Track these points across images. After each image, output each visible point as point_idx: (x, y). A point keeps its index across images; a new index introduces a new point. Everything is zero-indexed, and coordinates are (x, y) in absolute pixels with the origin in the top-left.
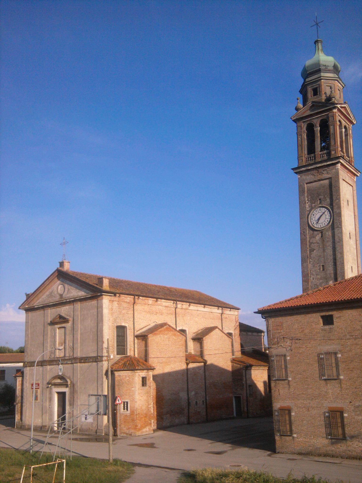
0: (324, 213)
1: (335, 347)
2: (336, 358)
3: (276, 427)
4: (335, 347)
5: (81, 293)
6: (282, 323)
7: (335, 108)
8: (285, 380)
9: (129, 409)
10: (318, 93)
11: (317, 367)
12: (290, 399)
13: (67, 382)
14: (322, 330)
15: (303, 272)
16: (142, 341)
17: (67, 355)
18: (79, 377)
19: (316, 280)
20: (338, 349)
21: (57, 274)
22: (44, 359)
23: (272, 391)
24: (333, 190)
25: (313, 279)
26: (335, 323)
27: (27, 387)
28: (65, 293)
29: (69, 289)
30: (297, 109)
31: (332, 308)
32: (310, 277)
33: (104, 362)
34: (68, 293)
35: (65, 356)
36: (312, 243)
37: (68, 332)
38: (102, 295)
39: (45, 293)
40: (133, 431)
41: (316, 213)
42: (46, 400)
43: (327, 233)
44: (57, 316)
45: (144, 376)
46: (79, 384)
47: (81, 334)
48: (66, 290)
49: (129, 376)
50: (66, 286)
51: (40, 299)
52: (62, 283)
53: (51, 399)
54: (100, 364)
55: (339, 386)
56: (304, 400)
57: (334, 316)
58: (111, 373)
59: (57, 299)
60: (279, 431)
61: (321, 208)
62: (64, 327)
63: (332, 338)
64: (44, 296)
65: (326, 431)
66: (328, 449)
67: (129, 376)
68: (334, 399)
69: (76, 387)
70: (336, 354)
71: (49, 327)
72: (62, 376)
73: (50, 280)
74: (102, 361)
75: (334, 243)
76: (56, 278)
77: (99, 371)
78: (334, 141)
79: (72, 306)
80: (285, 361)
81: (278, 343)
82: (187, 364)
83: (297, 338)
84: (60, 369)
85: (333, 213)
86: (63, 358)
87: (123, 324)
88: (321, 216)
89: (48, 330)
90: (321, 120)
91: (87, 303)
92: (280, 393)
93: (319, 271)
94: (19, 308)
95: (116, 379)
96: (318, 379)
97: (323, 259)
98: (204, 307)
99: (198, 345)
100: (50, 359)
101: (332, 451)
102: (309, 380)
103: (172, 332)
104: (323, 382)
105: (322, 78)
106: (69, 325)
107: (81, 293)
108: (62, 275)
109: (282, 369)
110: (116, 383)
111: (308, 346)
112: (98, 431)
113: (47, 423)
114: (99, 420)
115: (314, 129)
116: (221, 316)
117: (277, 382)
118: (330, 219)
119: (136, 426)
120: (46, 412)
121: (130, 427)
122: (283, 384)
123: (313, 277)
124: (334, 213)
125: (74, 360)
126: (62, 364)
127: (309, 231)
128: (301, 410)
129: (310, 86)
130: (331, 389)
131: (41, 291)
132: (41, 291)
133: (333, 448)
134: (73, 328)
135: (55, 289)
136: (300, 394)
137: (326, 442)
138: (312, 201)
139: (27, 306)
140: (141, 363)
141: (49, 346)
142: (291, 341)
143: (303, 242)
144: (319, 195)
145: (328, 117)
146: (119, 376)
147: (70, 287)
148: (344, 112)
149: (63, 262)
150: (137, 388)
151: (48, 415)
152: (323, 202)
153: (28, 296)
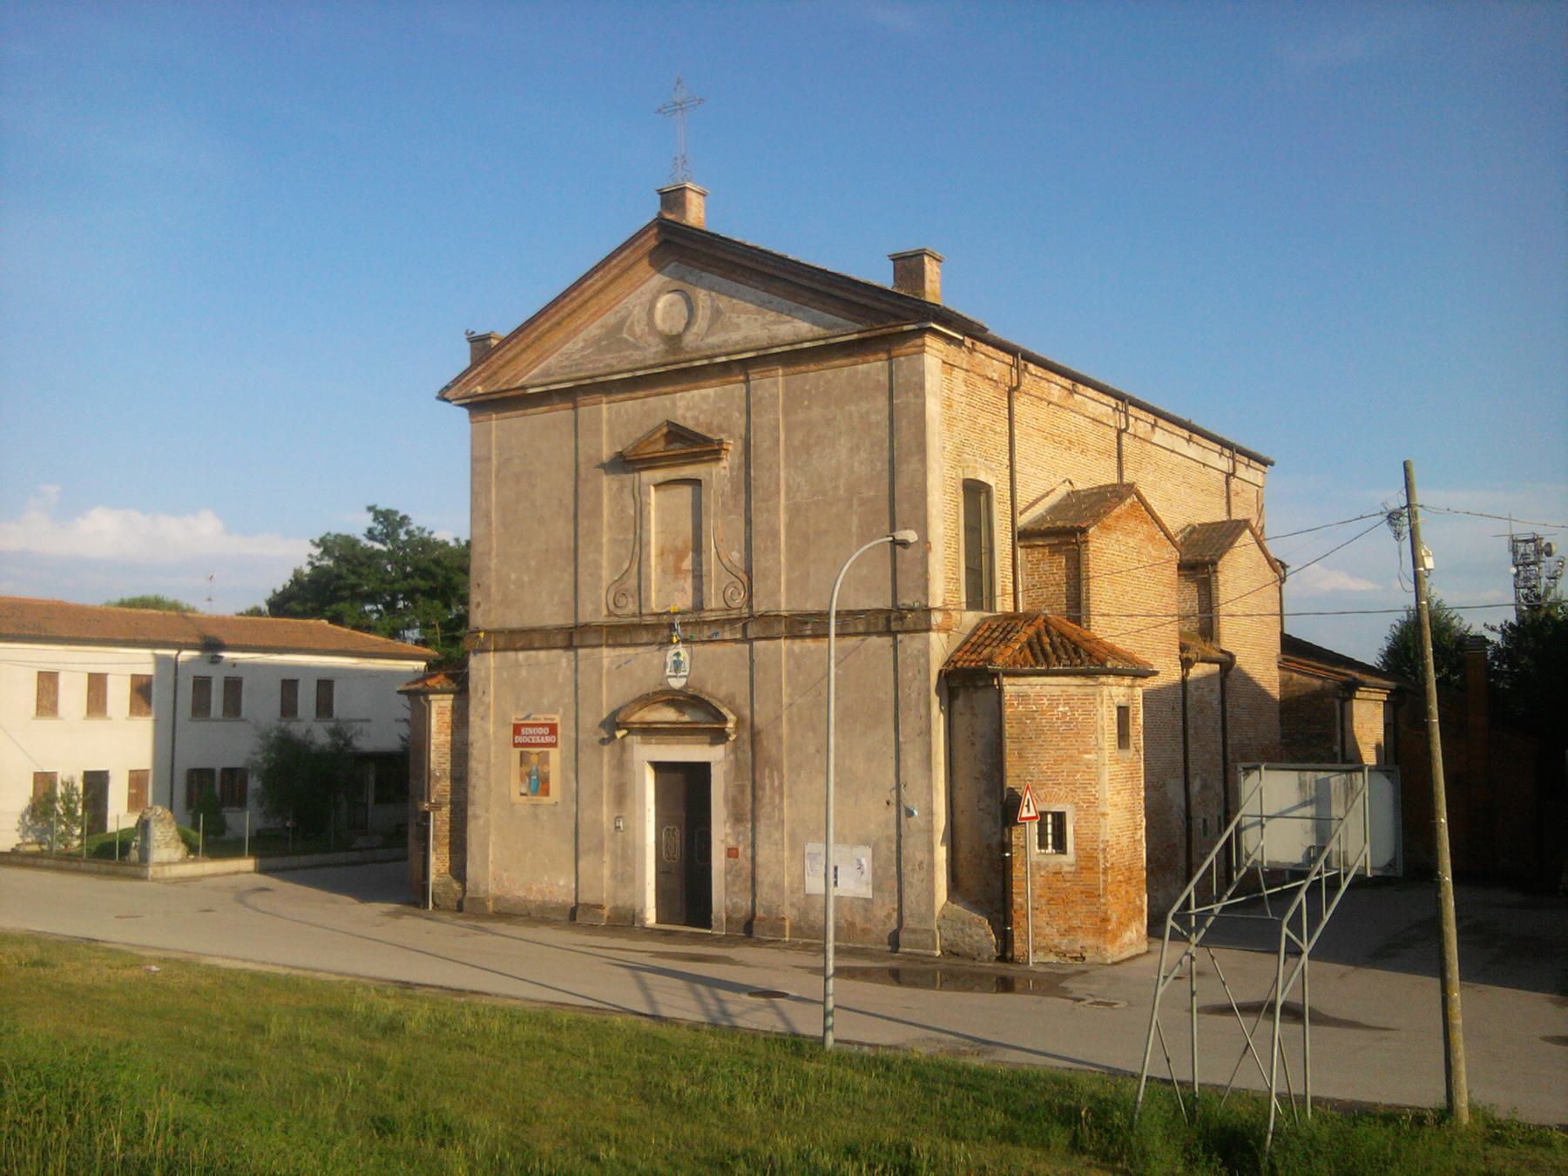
5: (797, 328)
9: (1070, 846)
13: (725, 720)
16: (1052, 553)
17: (713, 601)
18: (785, 700)
21: (653, 243)
22: (582, 620)
27: (486, 735)
28: (695, 329)
29: (717, 313)
33: (933, 636)
34: (710, 330)
35: (699, 606)
37: (711, 503)
38: (921, 332)
39: (576, 332)
40: (1090, 941)
42: (597, 795)
44: (659, 428)
45: (1123, 701)
46: (785, 729)
47: (795, 511)
48: (703, 315)
49: (1068, 700)
50: (702, 297)
51: (552, 361)
52: (676, 284)
53: (622, 794)
54: (911, 644)
58: (967, 683)
59: (651, 353)
62: (696, 483)
64: (575, 346)
67: (1068, 700)
69: (767, 743)
71: (607, 483)
72: (691, 691)
73: (615, 271)
74: (928, 629)
76: (646, 262)
77: (907, 674)
79: (736, 389)
82: (1186, 664)
84: (678, 665)
86: (690, 618)
87: (982, 478)
89: (599, 494)
91: (829, 374)
94: (442, 397)
95: (1008, 711)
98: (1189, 440)
99: (1191, 591)
100: (614, 620)
106: (719, 474)
107: (797, 328)
108: (678, 246)
110: (1009, 730)
112: (904, 936)
113: (602, 888)
114: (907, 891)
116: (1228, 484)
119: (1105, 920)
120: (599, 848)
121: (1076, 922)
125: (754, 625)
126: (685, 641)
131: (559, 324)
132: (559, 324)
134: (746, 485)
135: (639, 313)
139: (480, 389)
140: (1068, 649)
141: (605, 563)
146: (1023, 698)
147: (723, 302)
148: (536, 371)
149: (682, 190)
151: (607, 858)
153: (482, 347)
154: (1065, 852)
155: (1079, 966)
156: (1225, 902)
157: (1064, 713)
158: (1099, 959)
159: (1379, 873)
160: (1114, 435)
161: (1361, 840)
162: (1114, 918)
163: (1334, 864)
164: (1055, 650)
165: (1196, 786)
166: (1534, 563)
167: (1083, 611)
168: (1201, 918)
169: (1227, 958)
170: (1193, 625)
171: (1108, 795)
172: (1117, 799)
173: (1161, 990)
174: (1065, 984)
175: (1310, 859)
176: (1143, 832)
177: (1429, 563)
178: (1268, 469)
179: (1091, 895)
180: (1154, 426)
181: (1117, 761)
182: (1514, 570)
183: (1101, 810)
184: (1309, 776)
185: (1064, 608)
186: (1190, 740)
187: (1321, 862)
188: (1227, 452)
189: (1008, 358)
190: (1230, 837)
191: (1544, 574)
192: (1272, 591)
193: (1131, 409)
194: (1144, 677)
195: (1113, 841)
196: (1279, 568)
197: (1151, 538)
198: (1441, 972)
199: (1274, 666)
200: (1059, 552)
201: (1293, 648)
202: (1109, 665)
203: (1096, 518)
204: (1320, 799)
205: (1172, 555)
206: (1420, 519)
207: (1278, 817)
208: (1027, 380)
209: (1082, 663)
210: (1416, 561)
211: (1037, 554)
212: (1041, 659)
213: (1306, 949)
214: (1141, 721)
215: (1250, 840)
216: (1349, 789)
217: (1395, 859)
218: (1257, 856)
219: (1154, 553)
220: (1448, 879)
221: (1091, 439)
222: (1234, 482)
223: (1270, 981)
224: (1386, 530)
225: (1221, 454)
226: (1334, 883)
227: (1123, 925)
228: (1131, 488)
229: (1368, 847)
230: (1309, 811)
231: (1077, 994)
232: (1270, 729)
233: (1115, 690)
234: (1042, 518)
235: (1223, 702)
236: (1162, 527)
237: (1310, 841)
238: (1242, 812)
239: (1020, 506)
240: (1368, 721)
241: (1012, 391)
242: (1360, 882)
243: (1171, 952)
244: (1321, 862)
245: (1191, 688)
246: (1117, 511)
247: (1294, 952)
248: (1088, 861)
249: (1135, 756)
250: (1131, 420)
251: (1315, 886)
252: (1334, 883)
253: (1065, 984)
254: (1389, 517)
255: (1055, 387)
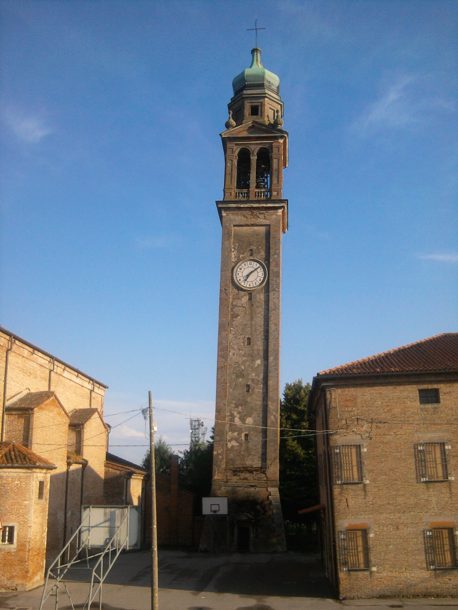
0: (256, 269)
1: (441, 434)
2: (443, 452)
3: (340, 557)
4: (441, 434)
6: (355, 398)
7: (282, 137)
8: (358, 483)
10: (259, 114)
11: (413, 464)
12: (367, 513)
14: (422, 410)
15: (220, 343)
16: (19, 418)
19: (238, 357)
20: (446, 438)
23: (336, 501)
24: (271, 242)
25: (234, 354)
26: (441, 401)
30: (228, 125)
31: (440, 379)
32: (230, 352)
36: (236, 306)
40: (20, 581)
41: (245, 267)
43: (258, 296)
55: (448, 490)
56: (390, 513)
57: (440, 390)
60: (345, 564)
61: (253, 262)
63: (437, 421)
65: (426, 558)
66: (429, 585)
68: (439, 510)
70: (443, 445)
75: (267, 309)
78: (277, 178)
80: (359, 454)
81: (347, 427)
82: (69, 464)
83: (380, 420)
85: (269, 271)
88: (252, 272)
90: (261, 149)
92: (350, 504)
93: (242, 344)
96: (414, 481)
97: (249, 329)
98: (77, 376)
99: (73, 435)
101: (436, 588)
102: (399, 483)
103: (57, 409)
104: (423, 486)
105: (267, 95)
109: (436, 464)
111: (399, 433)
115: (250, 157)
116: (91, 394)
117: (345, 486)
118: (264, 278)
119: (27, 572)
121: (15, 574)
122: (354, 490)
123: (233, 352)
124: (271, 272)
127: (232, 289)
128: (385, 529)
129: (249, 101)
130: (435, 496)
133: (438, 584)
136: (383, 505)
137: (426, 574)
138: (240, 250)
142: (370, 425)
143: (223, 302)
144: (251, 244)
145: (271, 147)
150: (33, 501)
152: (255, 254)
154: (13, 544)
155: (15, 593)
156: (72, 562)
157: (17, 484)
158: (23, 589)
159: (131, 548)
160: (48, 372)
161: (125, 536)
162: (31, 571)
163: (115, 545)
164: (16, 458)
165: (69, 514)
166: (197, 429)
167: (29, 442)
168: (62, 570)
169: (73, 586)
170: (73, 449)
171: (32, 519)
172: (36, 520)
173: (43, 602)
174: (7, 602)
175: (106, 544)
176: (46, 534)
177: (155, 429)
178: (106, 390)
179: (22, 561)
180: (64, 370)
181: (37, 504)
182: (191, 431)
183: (29, 525)
184: (108, 510)
185: (22, 440)
186: (68, 495)
187: (110, 544)
188: (91, 382)
189: (8, 337)
190: (76, 537)
191: (201, 432)
192: (104, 436)
193: (56, 362)
194: (51, 469)
195: (33, 538)
196: (107, 427)
197: (59, 414)
198: (152, 585)
199: (103, 465)
200: (22, 417)
201: (111, 459)
202: (37, 464)
203: (38, 404)
204: (111, 519)
205: (67, 421)
206: (153, 412)
207: (97, 527)
208: (14, 347)
209: (27, 463)
210: (151, 428)
211: (12, 418)
212: (10, 461)
213: (102, 580)
214: (48, 487)
215: (84, 536)
216: (122, 515)
217: (137, 542)
218: (86, 543)
219: (60, 420)
220: (156, 549)
221: (38, 373)
222: (93, 394)
223: (87, 596)
224: (141, 416)
225: (89, 383)
226: (114, 552)
227: (34, 574)
228: (53, 394)
229: (128, 538)
230: (107, 524)
231: (11, 606)
232: (99, 491)
233: (39, 475)
234: (16, 403)
235: (82, 480)
236: (64, 410)
237: (107, 536)
238: (81, 525)
239: (8, 397)
240: (136, 488)
241: (8, 351)
242: (124, 551)
243: (51, 584)
244: (110, 544)
245: (70, 474)
246: (46, 402)
247: (97, 581)
248: (22, 547)
249: (45, 503)
250: (55, 367)
251: (107, 555)
252: (114, 552)
253: (7, 602)
254: (143, 411)
255: (26, 351)
